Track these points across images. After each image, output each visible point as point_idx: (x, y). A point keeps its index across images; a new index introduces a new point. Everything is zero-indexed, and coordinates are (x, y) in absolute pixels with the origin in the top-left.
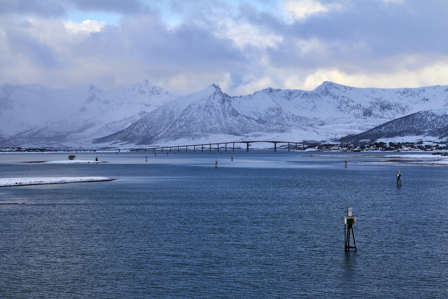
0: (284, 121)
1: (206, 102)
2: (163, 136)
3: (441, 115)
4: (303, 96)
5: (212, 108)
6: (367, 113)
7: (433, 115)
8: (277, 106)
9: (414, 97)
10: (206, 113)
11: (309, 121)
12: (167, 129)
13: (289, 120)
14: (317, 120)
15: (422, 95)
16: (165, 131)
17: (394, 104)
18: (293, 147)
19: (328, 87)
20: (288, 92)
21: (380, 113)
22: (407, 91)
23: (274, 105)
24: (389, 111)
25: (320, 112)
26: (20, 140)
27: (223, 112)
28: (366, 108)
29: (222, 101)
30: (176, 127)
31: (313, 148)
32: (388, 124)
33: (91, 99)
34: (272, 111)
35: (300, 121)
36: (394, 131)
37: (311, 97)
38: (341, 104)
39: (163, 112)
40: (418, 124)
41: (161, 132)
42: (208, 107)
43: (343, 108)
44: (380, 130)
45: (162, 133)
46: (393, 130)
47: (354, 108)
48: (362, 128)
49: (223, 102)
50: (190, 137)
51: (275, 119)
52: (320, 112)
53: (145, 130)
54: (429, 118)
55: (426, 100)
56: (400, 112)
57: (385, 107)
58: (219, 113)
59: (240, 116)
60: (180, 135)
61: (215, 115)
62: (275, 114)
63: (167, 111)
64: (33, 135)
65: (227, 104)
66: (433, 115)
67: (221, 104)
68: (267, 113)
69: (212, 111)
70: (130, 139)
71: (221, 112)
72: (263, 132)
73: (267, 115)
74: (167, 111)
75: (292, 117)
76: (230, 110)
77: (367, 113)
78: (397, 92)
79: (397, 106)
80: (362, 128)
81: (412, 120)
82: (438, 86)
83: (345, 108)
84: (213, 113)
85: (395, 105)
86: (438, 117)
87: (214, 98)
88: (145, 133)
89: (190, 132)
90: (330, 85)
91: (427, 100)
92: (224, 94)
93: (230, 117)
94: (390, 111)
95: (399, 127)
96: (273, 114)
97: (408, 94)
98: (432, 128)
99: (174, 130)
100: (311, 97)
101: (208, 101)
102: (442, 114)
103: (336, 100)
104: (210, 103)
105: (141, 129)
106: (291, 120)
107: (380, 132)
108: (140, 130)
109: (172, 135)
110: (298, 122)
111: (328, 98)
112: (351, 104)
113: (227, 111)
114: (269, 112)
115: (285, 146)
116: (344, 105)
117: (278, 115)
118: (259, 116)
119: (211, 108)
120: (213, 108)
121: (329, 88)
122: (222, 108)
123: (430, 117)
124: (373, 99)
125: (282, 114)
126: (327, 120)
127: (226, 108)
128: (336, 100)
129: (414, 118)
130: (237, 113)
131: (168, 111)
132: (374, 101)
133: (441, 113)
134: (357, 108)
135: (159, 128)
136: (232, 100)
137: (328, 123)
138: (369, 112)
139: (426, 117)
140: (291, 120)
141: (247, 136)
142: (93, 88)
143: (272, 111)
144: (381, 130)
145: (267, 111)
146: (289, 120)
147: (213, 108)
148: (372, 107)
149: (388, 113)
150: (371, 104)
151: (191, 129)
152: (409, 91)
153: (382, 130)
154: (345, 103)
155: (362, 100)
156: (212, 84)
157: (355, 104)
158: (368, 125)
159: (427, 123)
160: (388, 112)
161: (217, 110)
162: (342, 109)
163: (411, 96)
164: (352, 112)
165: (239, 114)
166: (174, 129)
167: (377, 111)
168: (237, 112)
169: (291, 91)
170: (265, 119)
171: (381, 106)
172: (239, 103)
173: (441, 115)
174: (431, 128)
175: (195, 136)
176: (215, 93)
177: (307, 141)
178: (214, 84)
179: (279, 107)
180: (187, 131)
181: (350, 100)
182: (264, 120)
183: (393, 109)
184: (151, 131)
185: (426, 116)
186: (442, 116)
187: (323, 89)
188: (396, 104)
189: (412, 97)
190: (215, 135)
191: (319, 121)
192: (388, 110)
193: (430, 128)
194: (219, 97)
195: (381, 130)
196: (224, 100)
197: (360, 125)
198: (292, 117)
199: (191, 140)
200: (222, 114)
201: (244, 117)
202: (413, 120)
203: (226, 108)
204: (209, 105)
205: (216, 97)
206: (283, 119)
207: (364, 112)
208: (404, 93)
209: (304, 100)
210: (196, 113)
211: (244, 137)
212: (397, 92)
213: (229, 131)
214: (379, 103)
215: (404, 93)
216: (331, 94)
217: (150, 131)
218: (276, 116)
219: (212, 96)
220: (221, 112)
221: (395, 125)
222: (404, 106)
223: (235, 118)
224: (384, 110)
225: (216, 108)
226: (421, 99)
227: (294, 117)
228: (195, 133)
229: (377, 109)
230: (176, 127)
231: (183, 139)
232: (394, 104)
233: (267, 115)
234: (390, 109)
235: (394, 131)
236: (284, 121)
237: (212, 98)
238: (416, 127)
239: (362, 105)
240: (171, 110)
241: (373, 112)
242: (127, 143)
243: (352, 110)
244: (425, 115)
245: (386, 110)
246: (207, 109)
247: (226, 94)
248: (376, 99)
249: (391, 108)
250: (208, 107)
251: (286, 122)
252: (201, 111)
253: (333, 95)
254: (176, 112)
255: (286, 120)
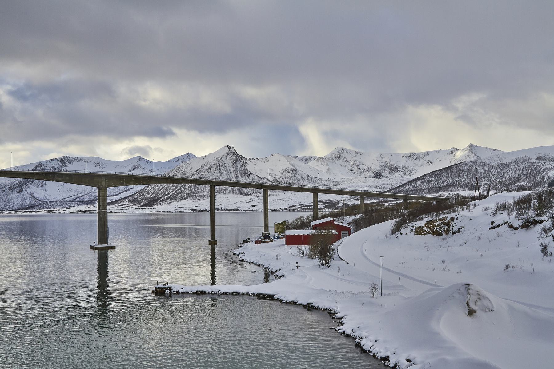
0: (299, 181)
1: (218, 162)
2: (170, 197)
3: (496, 165)
4: (318, 160)
5: (224, 168)
6: (378, 175)
7: (485, 165)
8: (292, 168)
9: (419, 160)
10: (217, 172)
11: (324, 181)
12: (177, 190)
13: (304, 181)
14: (331, 181)
15: (427, 158)
16: (174, 192)
17: (401, 167)
18: (304, 208)
19: (341, 152)
20: (304, 159)
21: (389, 175)
22: (413, 156)
23: (289, 167)
24: (397, 173)
25: (334, 174)
26: (52, 203)
27: (235, 172)
28: (376, 170)
29: (234, 161)
30: (185, 188)
31: (419, 231)
32: (424, 178)
33: (135, 168)
34: (287, 172)
35: (315, 181)
36: (435, 185)
37: (325, 160)
38: (353, 167)
39: (175, 173)
40: (467, 176)
41: (169, 193)
42: (219, 167)
43: (355, 170)
44: (415, 185)
45: (170, 194)
46: (434, 184)
47: (365, 171)
48: (379, 187)
49: (236, 162)
50: (197, 198)
51: (291, 179)
52: (334, 174)
53: (155, 191)
54: (480, 169)
55: (430, 162)
56: (407, 174)
57: (393, 169)
58: (231, 172)
59: (252, 176)
60: (186, 196)
61: (226, 175)
62: (290, 175)
63: (180, 172)
64: (74, 199)
65: (239, 164)
66: (485, 165)
67: (233, 163)
68: (282, 174)
69: (223, 171)
70: (138, 201)
71: (232, 171)
72: (276, 192)
73: (282, 175)
74: (180, 172)
75: (307, 178)
76: (243, 169)
77: (378, 175)
78: (403, 156)
79: (404, 168)
80: (379, 187)
81: (456, 171)
82: (440, 150)
83: (357, 170)
84: (225, 173)
85: (402, 168)
86: (492, 167)
87: (227, 158)
88: (154, 195)
89: (197, 192)
90: (342, 150)
91: (432, 163)
92: (240, 155)
93: (242, 177)
94: (398, 173)
95: (440, 181)
96: (289, 175)
97: (413, 158)
98: (488, 181)
99: (183, 191)
100: (325, 160)
101: (219, 161)
102: (497, 163)
103: (348, 163)
104: (222, 163)
105: (152, 191)
106: (306, 181)
107: (415, 188)
108: (150, 191)
109: (179, 196)
110: (313, 183)
111: (341, 162)
112: (361, 166)
113: (240, 171)
114: (284, 173)
115: (296, 207)
116: (356, 168)
117: (293, 176)
118: (274, 176)
119: (222, 168)
120: (225, 168)
121: (341, 153)
122: (234, 167)
123: (481, 167)
124: (382, 162)
125: (297, 175)
126: (341, 181)
127: (238, 168)
128: (348, 163)
129: (459, 168)
130: (250, 172)
131: (181, 172)
132: (383, 164)
133: (496, 163)
134: (368, 170)
135: (169, 189)
136: (248, 162)
137: (343, 183)
138: (379, 174)
139: (476, 167)
140: (306, 181)
141: (258, 196)
142: (141, 159)
143: (287, 172)
144: (416, 185)
145: (282, 172)
146: (304, 181)
147: (225, 168)
148: (381, 169)
149: (396, 175)
150: (380, 167)
151: (199, 189)
152: (414, 156)
153: (418, 185)
154: (357, 166)
155: (372, 164)
156: (226, 145)
157: (366, 167)
158: (384, 184)
159: (479, 175)
160: (396, 174)
161: (229, 170)
162: (354, 172)
163: (416, 159)
164: (363, 175)
165: (252, 174)
166: (182, 189)
167: (386, 173)
168: (250, 172)
169: (307, 158)
170: (280, 180)
171: (390, 169)
172: (255, 164)
173: (495, 165)
174: (486, 181)
175: (202, 196)
176: (228, 153)
177: (323, 200)
178: (228, 145)
179: (294, 168)
180: (194, 192)
181: (361, 163)
182: (279, 181)
183: (400, 171)
184: (161, 192)
185: (475, 166)
186: (498, 165)
187: (337, 154)
188: (403, 167)
189: (418, 160)
190: (224, 196)
191: (333, 182)
192: (396, 173)
193: (485, 180)
194: (231, 158)
195: (416, 185)
196: (236, 161)
197: (376, 184)
198: (307, 178)
199: (196, 200)
200: (233, 174)
201: (257, 177)
202: (459, 172)
203: (238, 168)
204: (220, 165)
205: (228, 157)
206: (298, 180)
207: (375, 174)
208: (410, 157)
209: (319, 163)
210: (206, 173)
211: (254, 197)
212: (403, 156)
213: (240, 191)
214: (388, 166)
215: (410, 157)
216: (343, 158)
217: (159, 193)
218: (291, 177)
219: (224, 156)
220: (232, 171)
221: (434, 178)
222: (410, 169)
223: (247, 178)
224: (392, 172)
225: (228, 168)
226: (426, 162)
227: (309, 177)
228: (203, 194)
229: (386, 172)
230: (185, 188)
231: (188, 200)
232: (401, 167)
233: (282, 175)
234: (398, 171)
235: (435, 185)
236: (299, 181)
237: (224, 159)
238: (465, 180)
239: (372, 168)
240: (183, 171)
241: (383, 174)
242: (135, 205)
243: (364, 172)
244: (474, 165)
245: (394, 172)
246: (218, 169)
247: (242, 156)
248: (385, 162)
249: (398, 171)
250: (219, 167)
251: (301, 183)
252: (212, 171)
253: (345, 159)
254: (188, 173)
255: (301, 180)
